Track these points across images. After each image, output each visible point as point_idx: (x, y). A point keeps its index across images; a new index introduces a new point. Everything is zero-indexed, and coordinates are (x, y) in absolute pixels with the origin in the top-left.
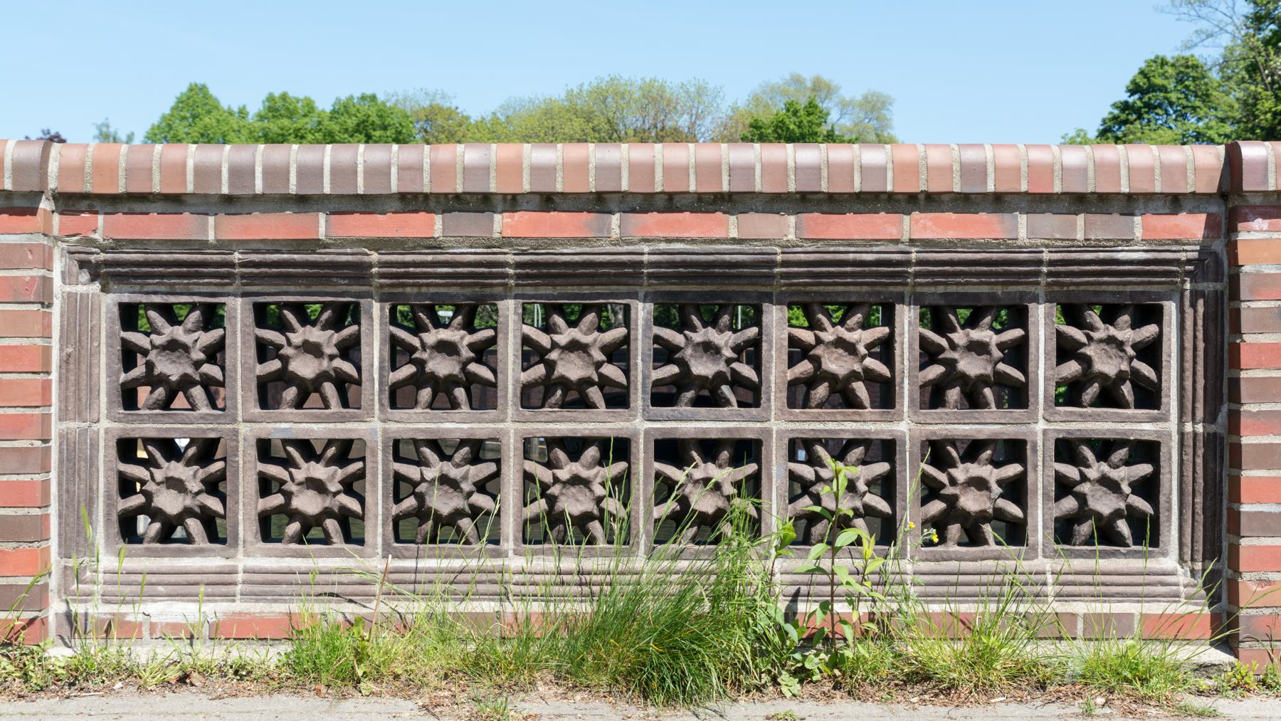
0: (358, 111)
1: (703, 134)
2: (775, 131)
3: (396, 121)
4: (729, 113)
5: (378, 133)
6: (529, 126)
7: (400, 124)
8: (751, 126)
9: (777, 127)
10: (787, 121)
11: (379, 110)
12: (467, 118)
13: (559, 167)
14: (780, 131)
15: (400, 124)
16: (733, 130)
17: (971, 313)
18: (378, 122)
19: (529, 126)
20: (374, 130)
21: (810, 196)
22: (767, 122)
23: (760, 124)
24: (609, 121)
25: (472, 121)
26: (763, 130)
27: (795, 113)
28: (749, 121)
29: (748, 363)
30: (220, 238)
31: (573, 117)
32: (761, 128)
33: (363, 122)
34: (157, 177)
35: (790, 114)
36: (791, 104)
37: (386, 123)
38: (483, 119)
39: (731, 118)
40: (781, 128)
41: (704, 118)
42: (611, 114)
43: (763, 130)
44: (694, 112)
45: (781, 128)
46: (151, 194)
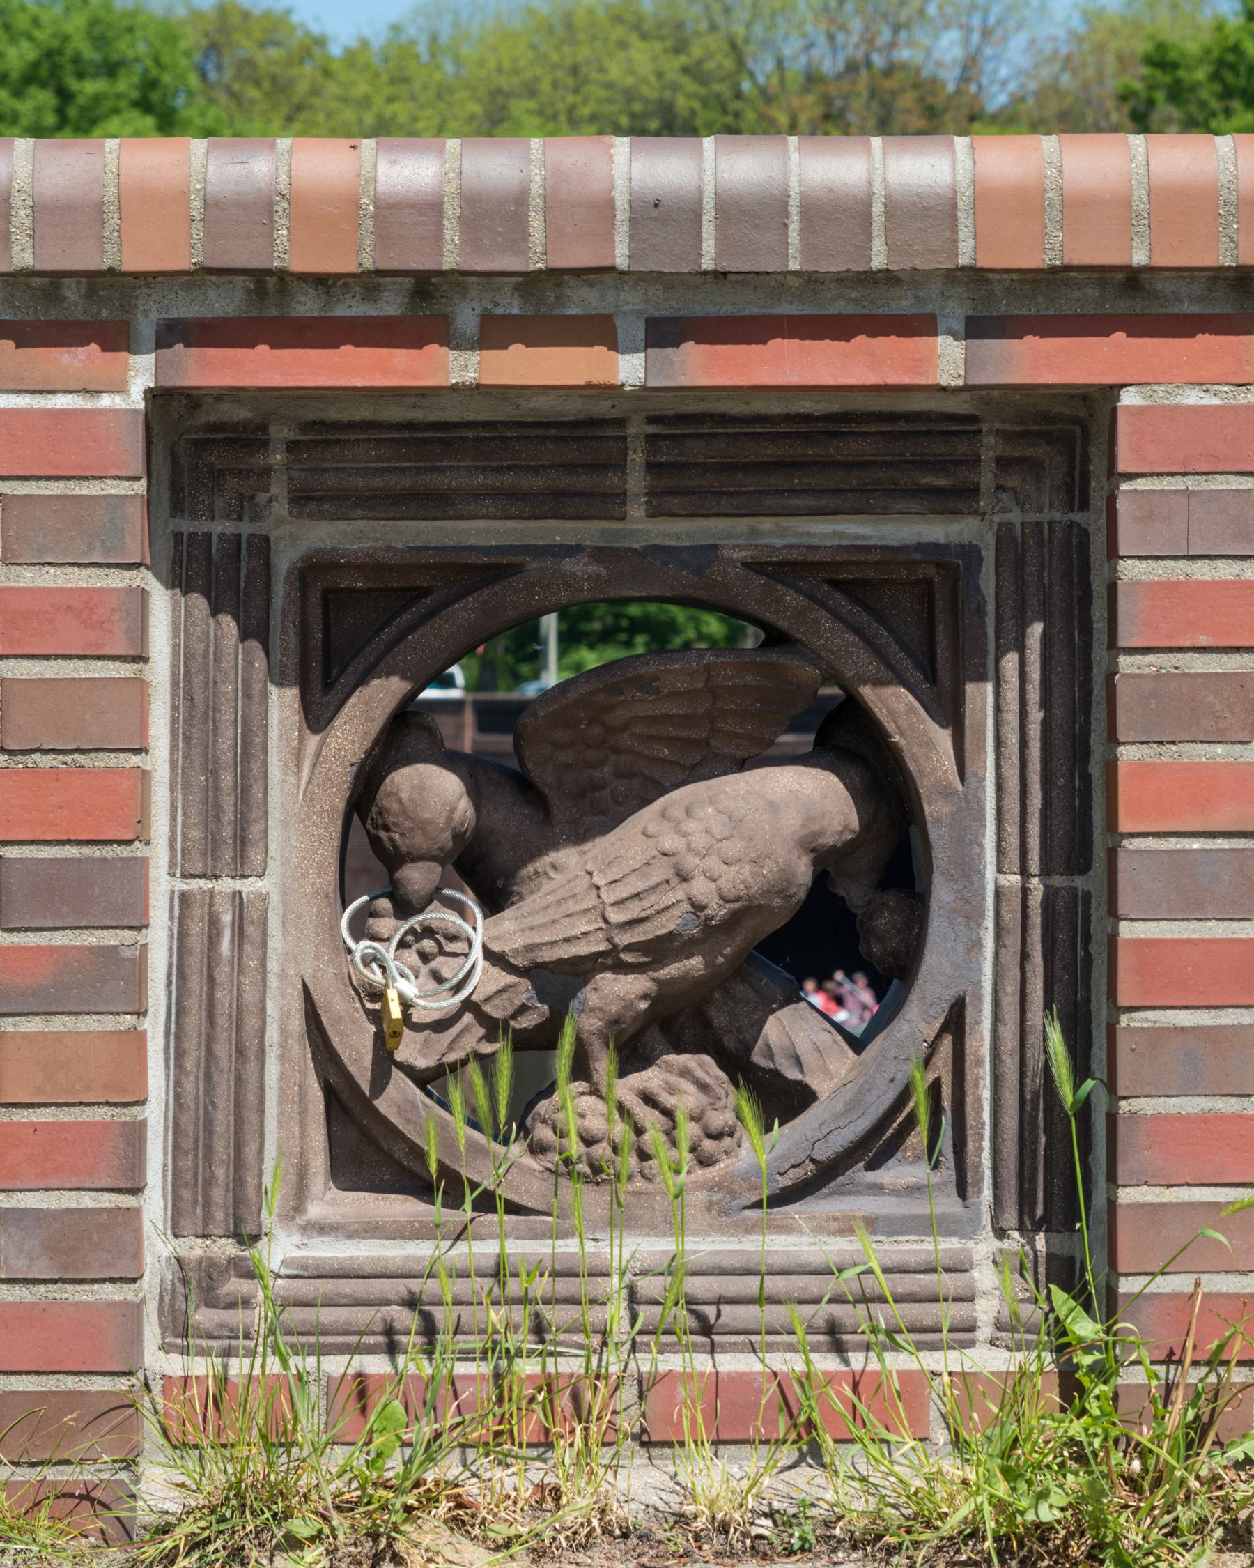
0: (36, 22)
1: (1004, 83)
2: (1216, 77)
3: (141, 48)
4: (1076, 23)
5: (90, 87)
6: (507, 65)
7: (157, 61)
8: (1149, 61)
9: (1221, 63)
11: (94, 22)
12: (321, 42)
13: (963, 202)
14: (1230, 78)
15: (157, 61)
16: (1090, 72)
17: (651, 1005)
18: (90, 54)
19: (507, 65)
20: (81, 76)
21: (991, 276)
22: (1192, 48)
23: (1173, 55)
24: (734, 46)
25: (335, 50)
26: (1182, 73)
28: (1143, 47)
29: (497, 1020)
30: (160, 384)
31: (634, 39)
32: (1174, 66)
33: (50, 54)
34: (452, 234)
37: (114, 57)
38: (365, 44)
39: (1080, 39)
40: (1233, 68)
41: (1005, 39)
42: (739, 30)
43: (1182, 73)
44: (976, 21)
45: (1233, 68)
46: (440, 273)
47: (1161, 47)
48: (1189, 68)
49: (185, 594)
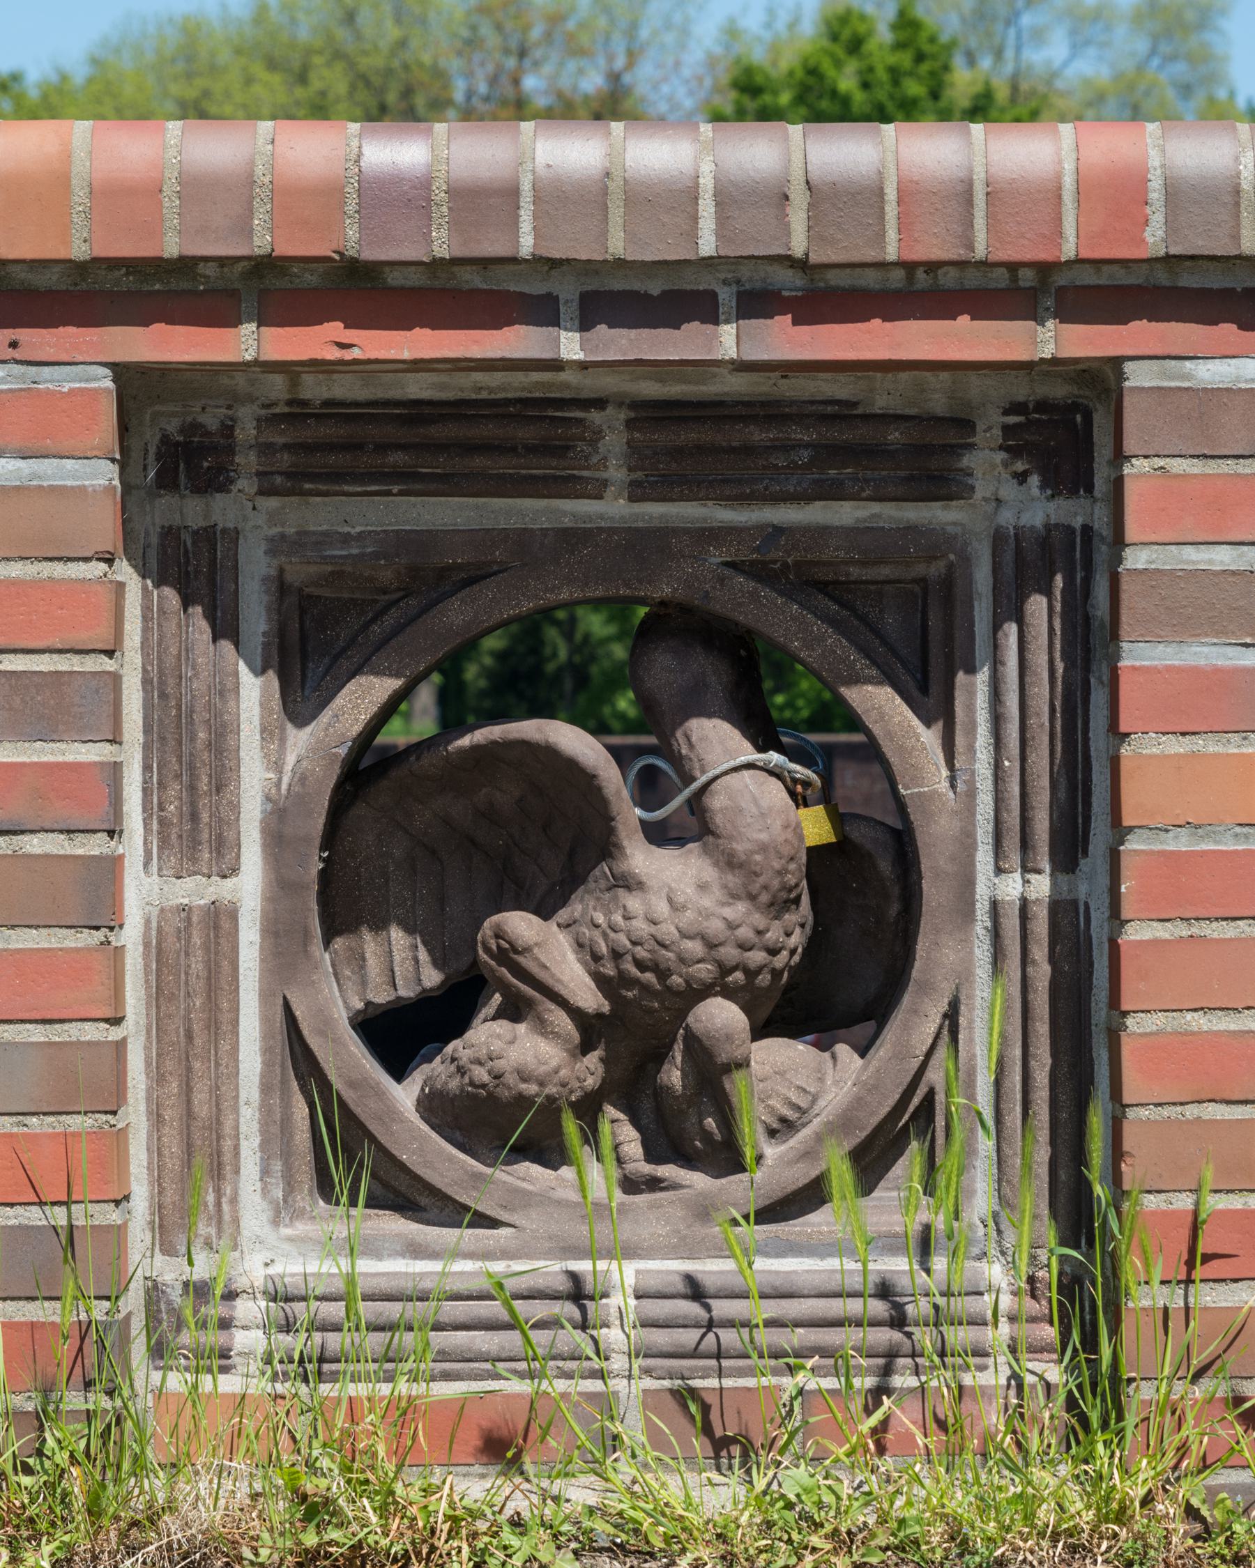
2: (800, 99)
10: (827, 67)
23: (759, 79)
27: (855, 46)
35: (840, 51)
36: (845, 18)
47: (749, 71)
48: (775, 93)
49: (157, 585)
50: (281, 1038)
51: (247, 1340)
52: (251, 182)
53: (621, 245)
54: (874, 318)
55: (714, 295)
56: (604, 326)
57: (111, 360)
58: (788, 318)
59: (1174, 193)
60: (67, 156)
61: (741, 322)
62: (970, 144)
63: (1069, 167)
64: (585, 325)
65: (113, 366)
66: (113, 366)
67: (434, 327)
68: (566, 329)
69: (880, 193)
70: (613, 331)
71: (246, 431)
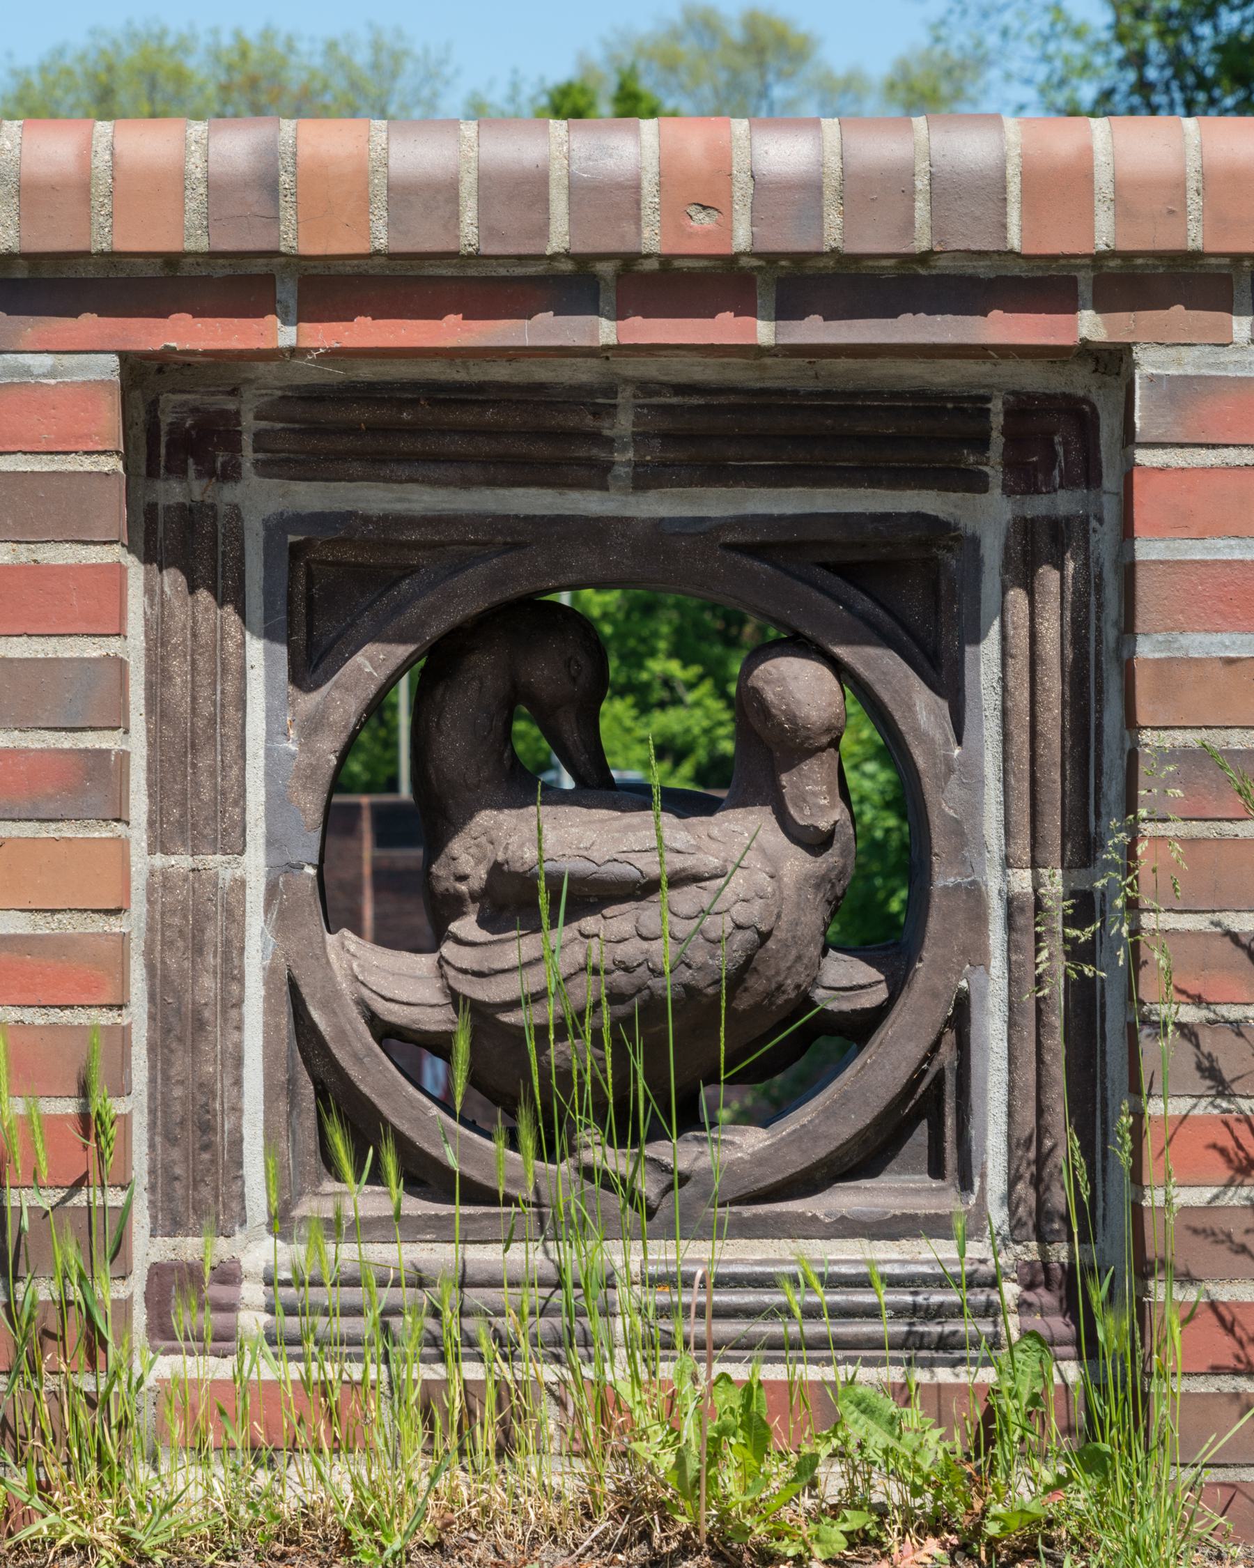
50: (285, 1020)
51: (252, 1321)
52: (182, 176)
53: (836, 234)
54: (814, 313)
55: (1074, 281)
56: (817, 317)
57: (116, 348)
58: (551, 313)
59: (578, 190)
60: (1087, 152)
61: (302, 325)
62: (822, 139)
63: (834, 164)
64: (1101, 306)
65: (120, 354)
66: (120, 354)
67: (955, 313)
68: (763, 319)
69: (637, 188)
70: (1192, 312)
71: (249, 423)
